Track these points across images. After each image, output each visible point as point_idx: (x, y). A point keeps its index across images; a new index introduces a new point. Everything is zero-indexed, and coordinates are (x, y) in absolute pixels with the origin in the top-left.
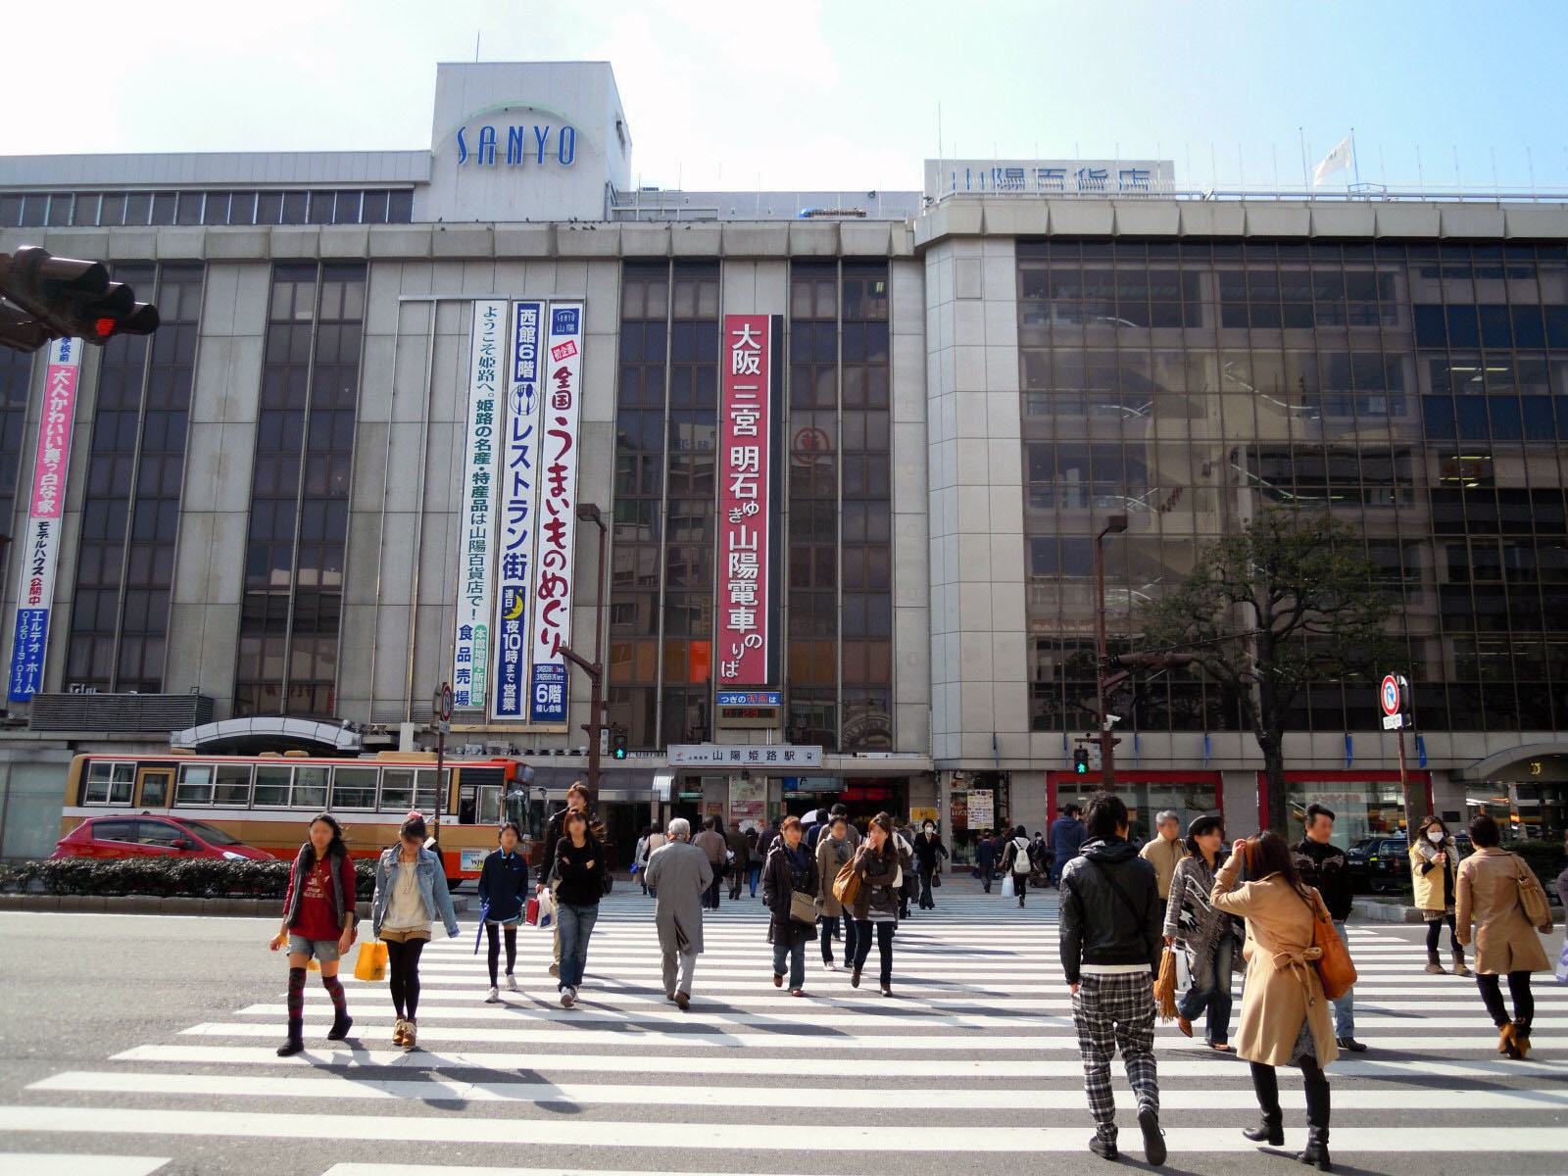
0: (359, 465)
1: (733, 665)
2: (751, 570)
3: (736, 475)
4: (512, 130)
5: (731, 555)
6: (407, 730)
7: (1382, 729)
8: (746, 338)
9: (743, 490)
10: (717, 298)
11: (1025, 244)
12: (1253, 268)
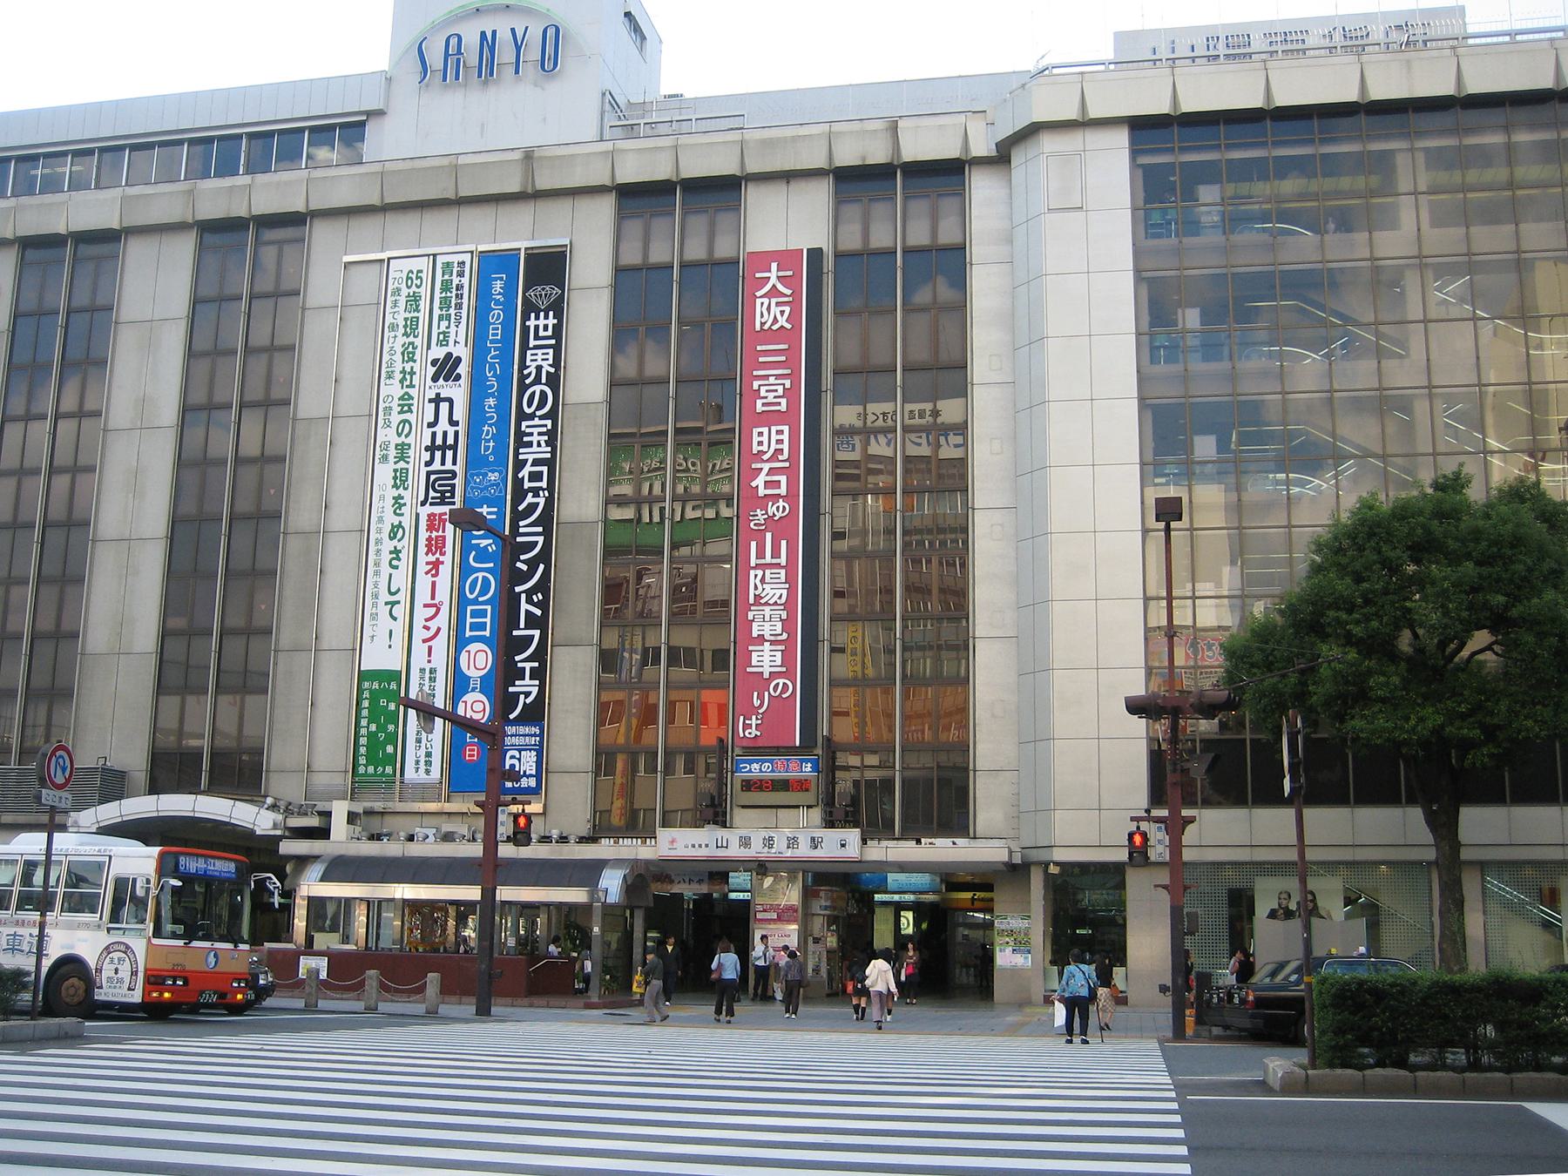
0: (295, 474)
1: (754, 722)
2: (778, 593)
3: (759, 466)
4: (483, 34)
5: (752, 573)
6: (340, 810)
8: (773, 280)
9: (767, 484)
10: (738, 231)
11: (1142, 127)
12: (1236, 155)
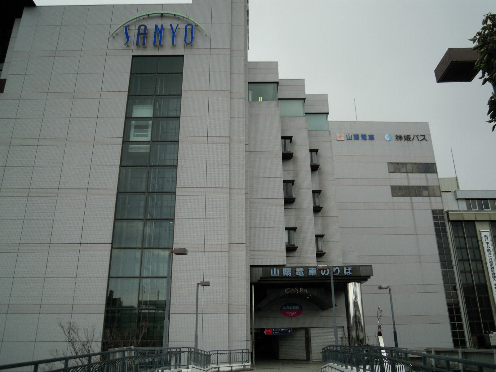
4: (156, 26)
7: (378, 328)
